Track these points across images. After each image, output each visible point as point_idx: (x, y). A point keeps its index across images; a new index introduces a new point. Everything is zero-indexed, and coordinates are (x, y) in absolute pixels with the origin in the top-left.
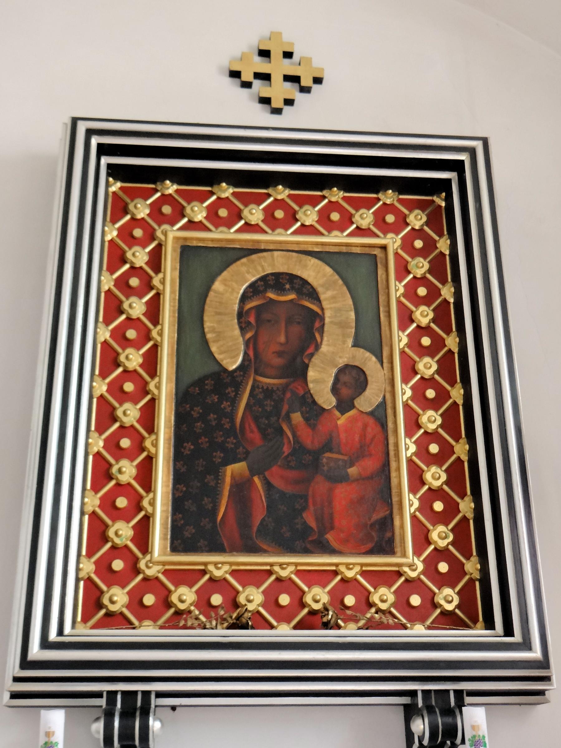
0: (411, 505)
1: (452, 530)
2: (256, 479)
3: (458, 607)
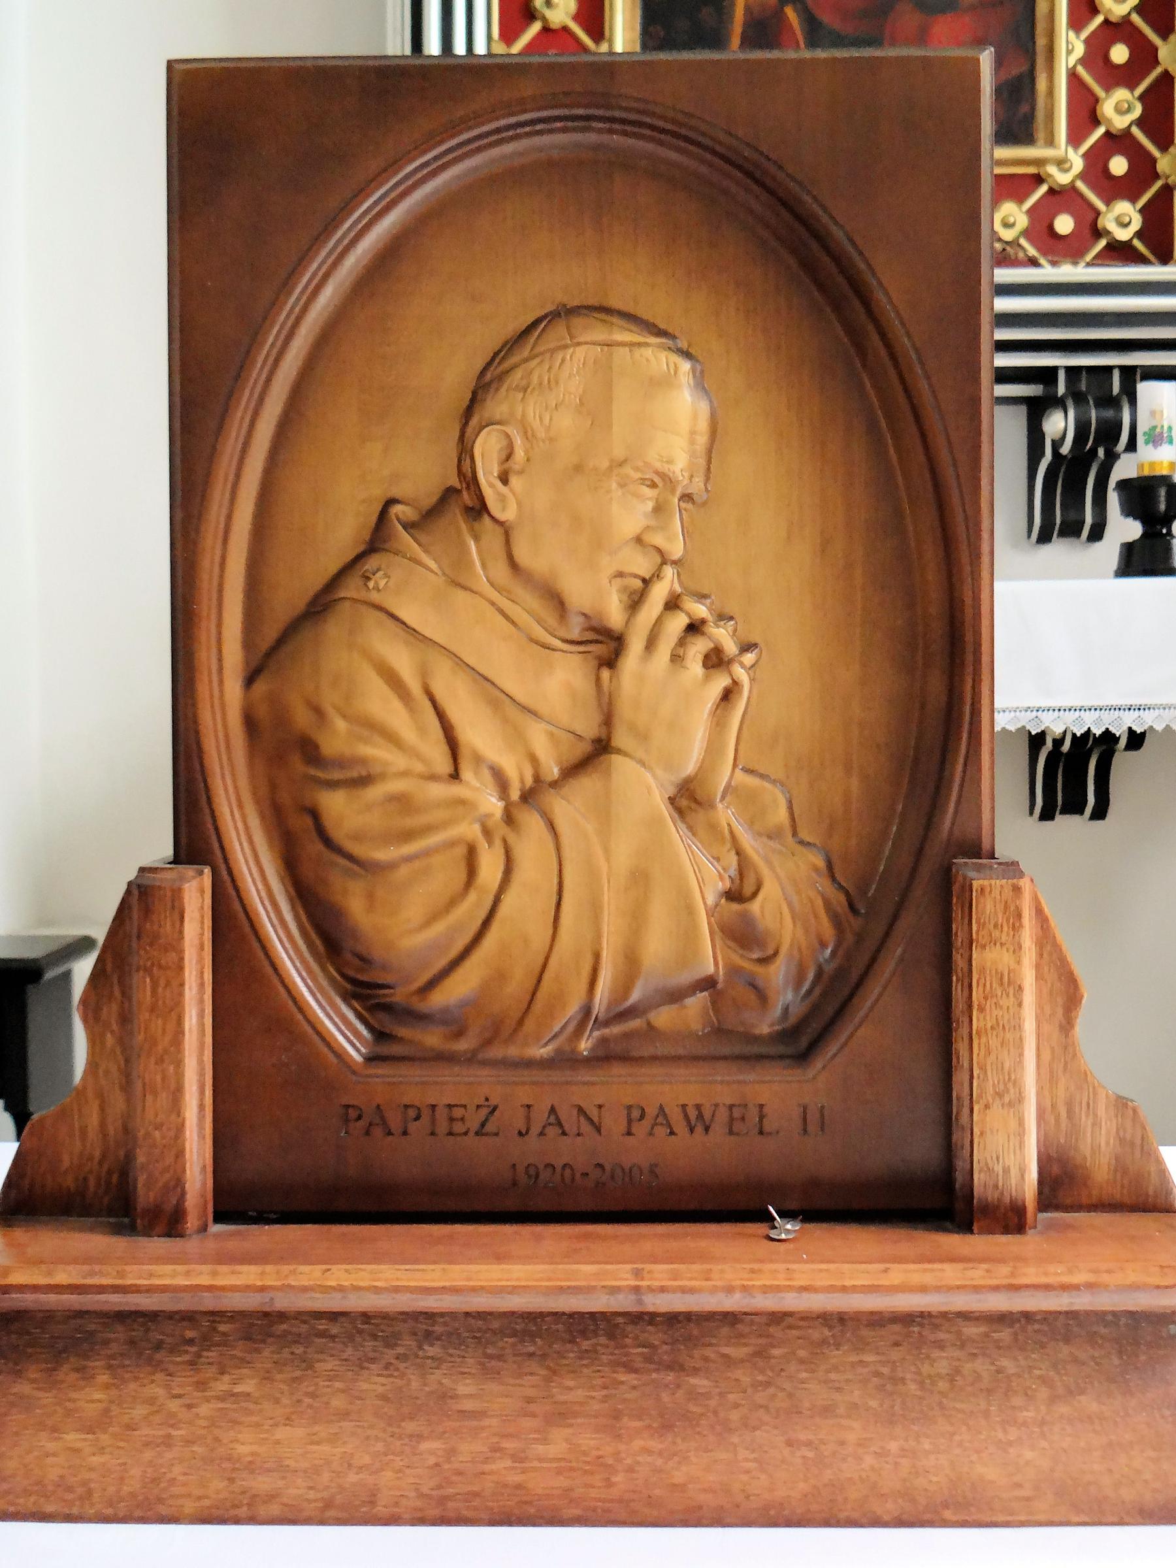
0: (1069, 52)
1: (1141, 98)
2: (790, 13)
3: (1139, 234)
